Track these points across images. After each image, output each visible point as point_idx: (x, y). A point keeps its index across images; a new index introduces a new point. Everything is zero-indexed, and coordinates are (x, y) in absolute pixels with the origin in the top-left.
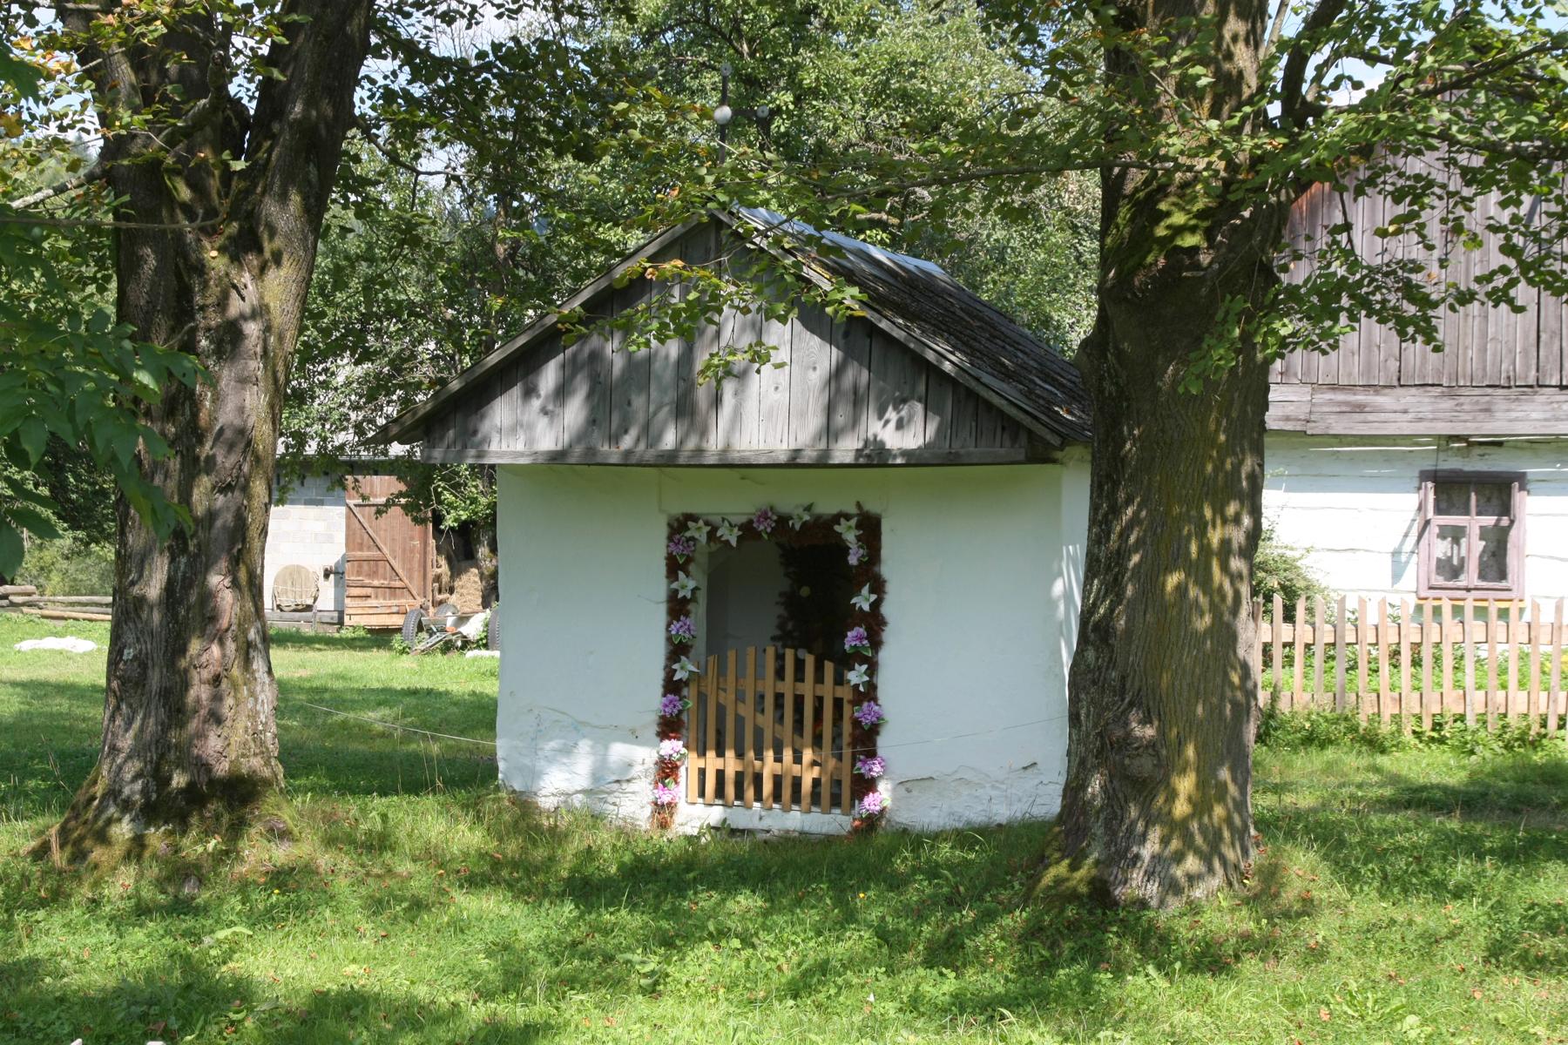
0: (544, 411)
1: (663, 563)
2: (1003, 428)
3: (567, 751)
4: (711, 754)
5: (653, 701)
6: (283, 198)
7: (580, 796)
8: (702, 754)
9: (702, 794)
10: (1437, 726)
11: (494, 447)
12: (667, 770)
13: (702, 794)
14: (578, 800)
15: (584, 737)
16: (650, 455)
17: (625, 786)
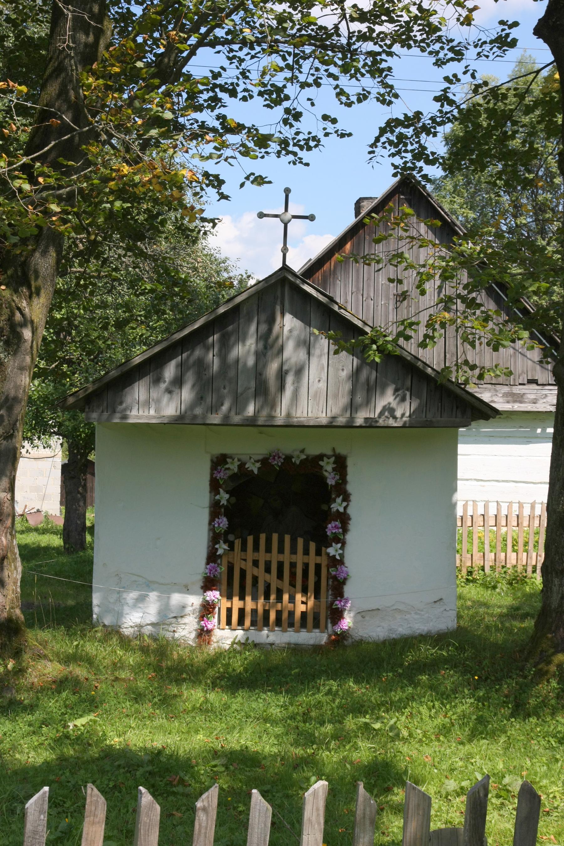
0: (169, 391)
1: (207, 483)
2: (457, 408)
3: (142, 599)
4: (236, 599)
5: (199, 566)
6: (44, 253)
7: (149, 627)
8: (230, 597)
9: (229, 623)
10: (470, 573)
11: (134, 412)
12: (207, 609)
13: (229, 623)
14: (148, 630)
15: (153, 590)
16: (236, 419)
17: (179, 620)
